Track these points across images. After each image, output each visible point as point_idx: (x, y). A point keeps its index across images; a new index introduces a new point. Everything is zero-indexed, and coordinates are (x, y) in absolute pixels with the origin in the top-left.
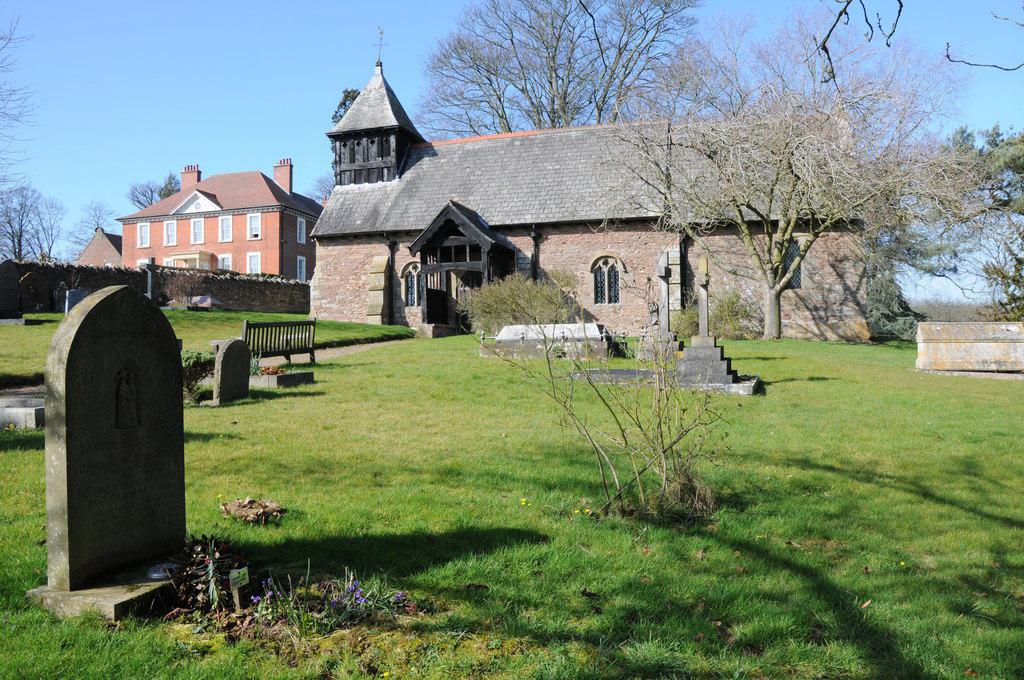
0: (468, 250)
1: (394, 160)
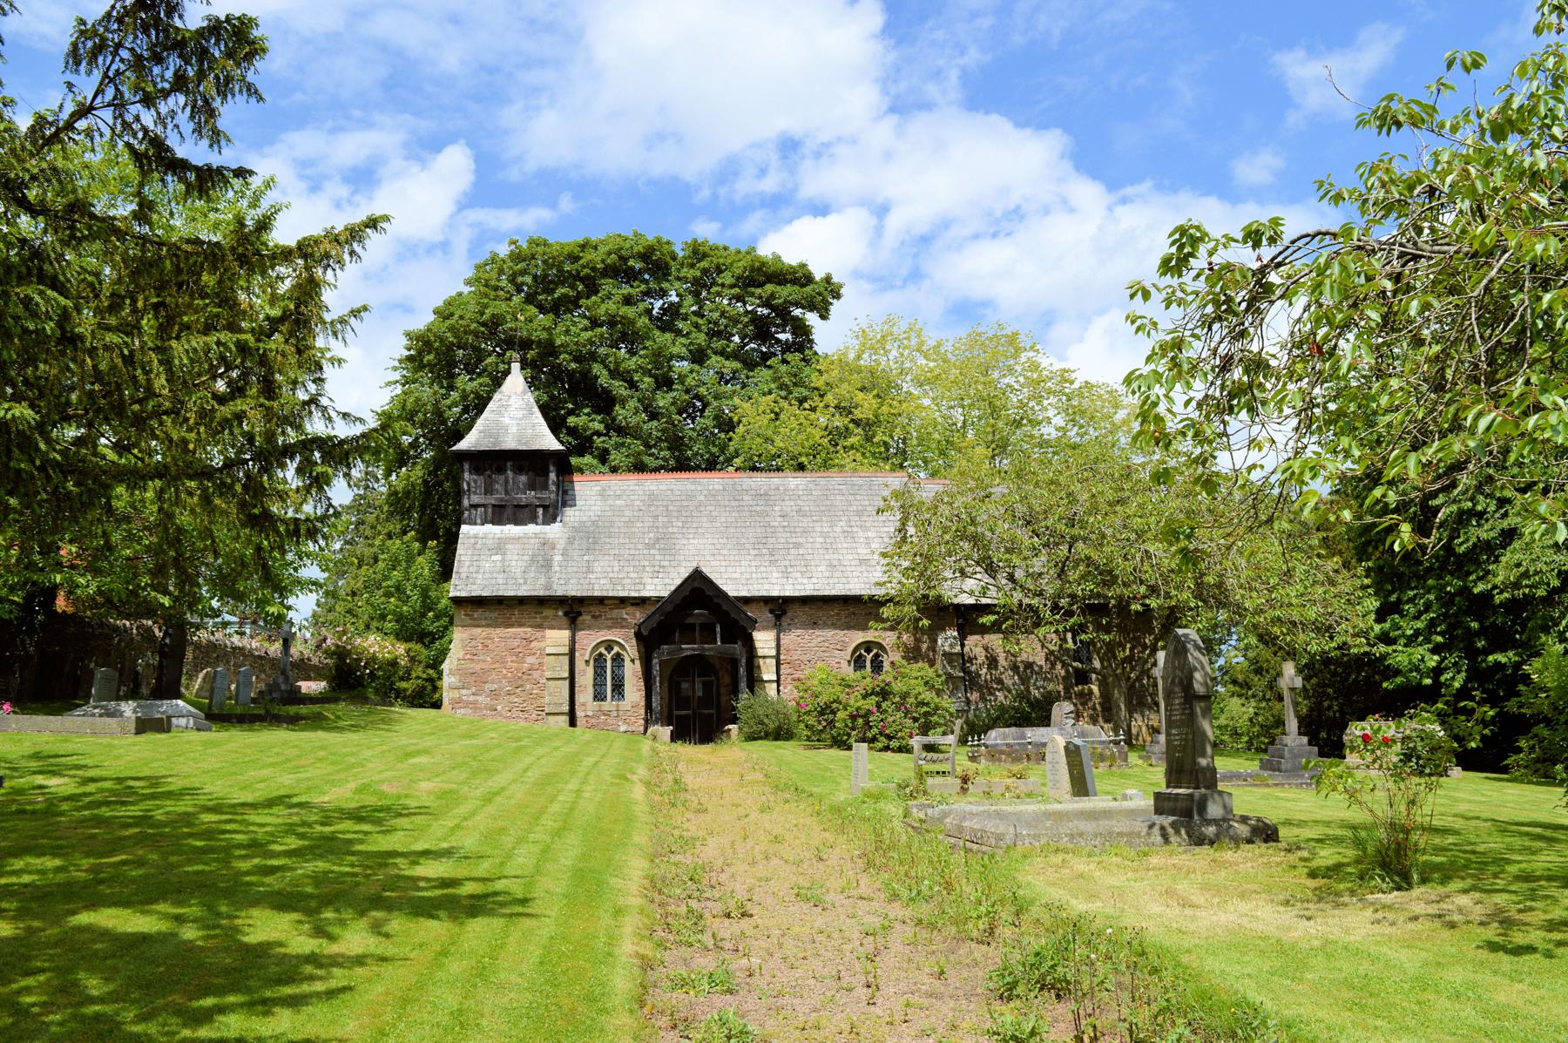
0: (718, 629)
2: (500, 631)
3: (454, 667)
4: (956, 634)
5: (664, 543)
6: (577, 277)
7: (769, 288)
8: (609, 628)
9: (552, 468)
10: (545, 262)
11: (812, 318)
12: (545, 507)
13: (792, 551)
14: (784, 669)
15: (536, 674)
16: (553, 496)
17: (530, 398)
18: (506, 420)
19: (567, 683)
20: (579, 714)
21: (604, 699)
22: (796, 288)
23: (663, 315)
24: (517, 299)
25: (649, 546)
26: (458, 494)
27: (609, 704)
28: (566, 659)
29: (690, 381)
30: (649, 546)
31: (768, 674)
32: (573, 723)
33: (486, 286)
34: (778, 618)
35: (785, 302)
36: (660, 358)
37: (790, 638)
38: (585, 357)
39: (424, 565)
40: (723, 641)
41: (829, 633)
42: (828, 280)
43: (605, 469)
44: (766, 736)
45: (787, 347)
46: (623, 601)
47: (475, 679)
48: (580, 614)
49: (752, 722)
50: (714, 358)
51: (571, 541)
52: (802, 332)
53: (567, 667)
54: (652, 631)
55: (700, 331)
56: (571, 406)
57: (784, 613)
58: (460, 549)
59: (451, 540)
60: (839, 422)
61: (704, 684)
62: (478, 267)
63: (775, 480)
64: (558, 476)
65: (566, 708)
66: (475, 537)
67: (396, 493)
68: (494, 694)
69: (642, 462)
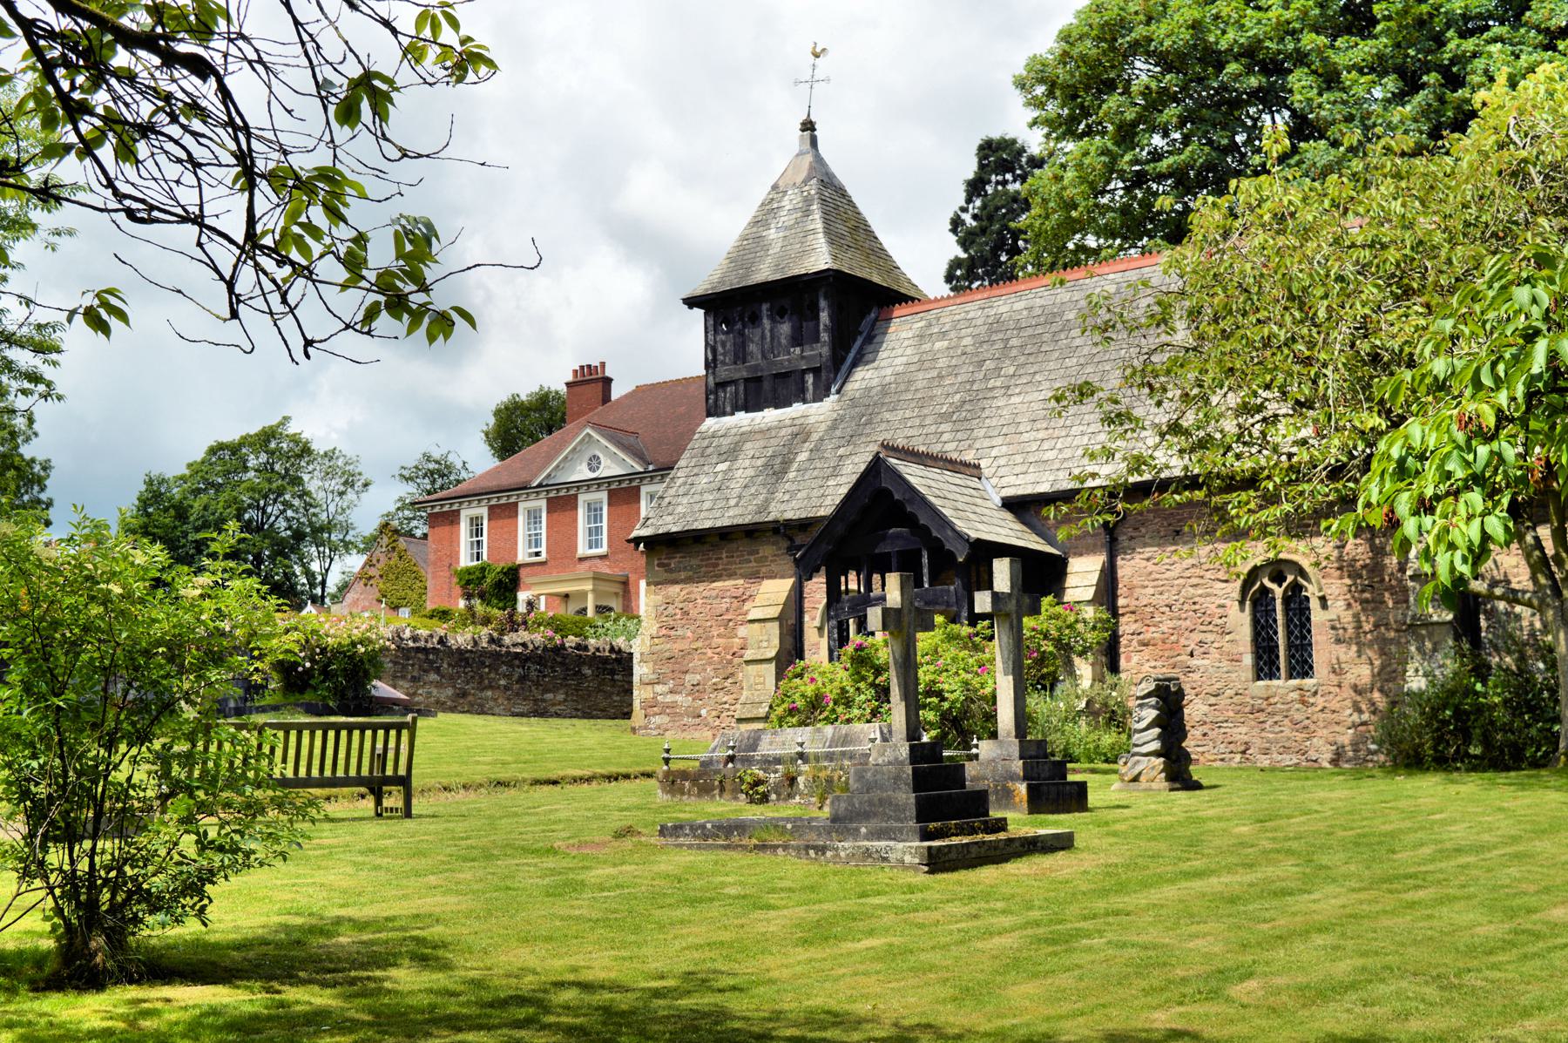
0: (925, 560)
1: (825, 351)
2: (701, 590)
3: (646, 650)
9: (823, 303)
12: (816, 371)
68: (697, 690)
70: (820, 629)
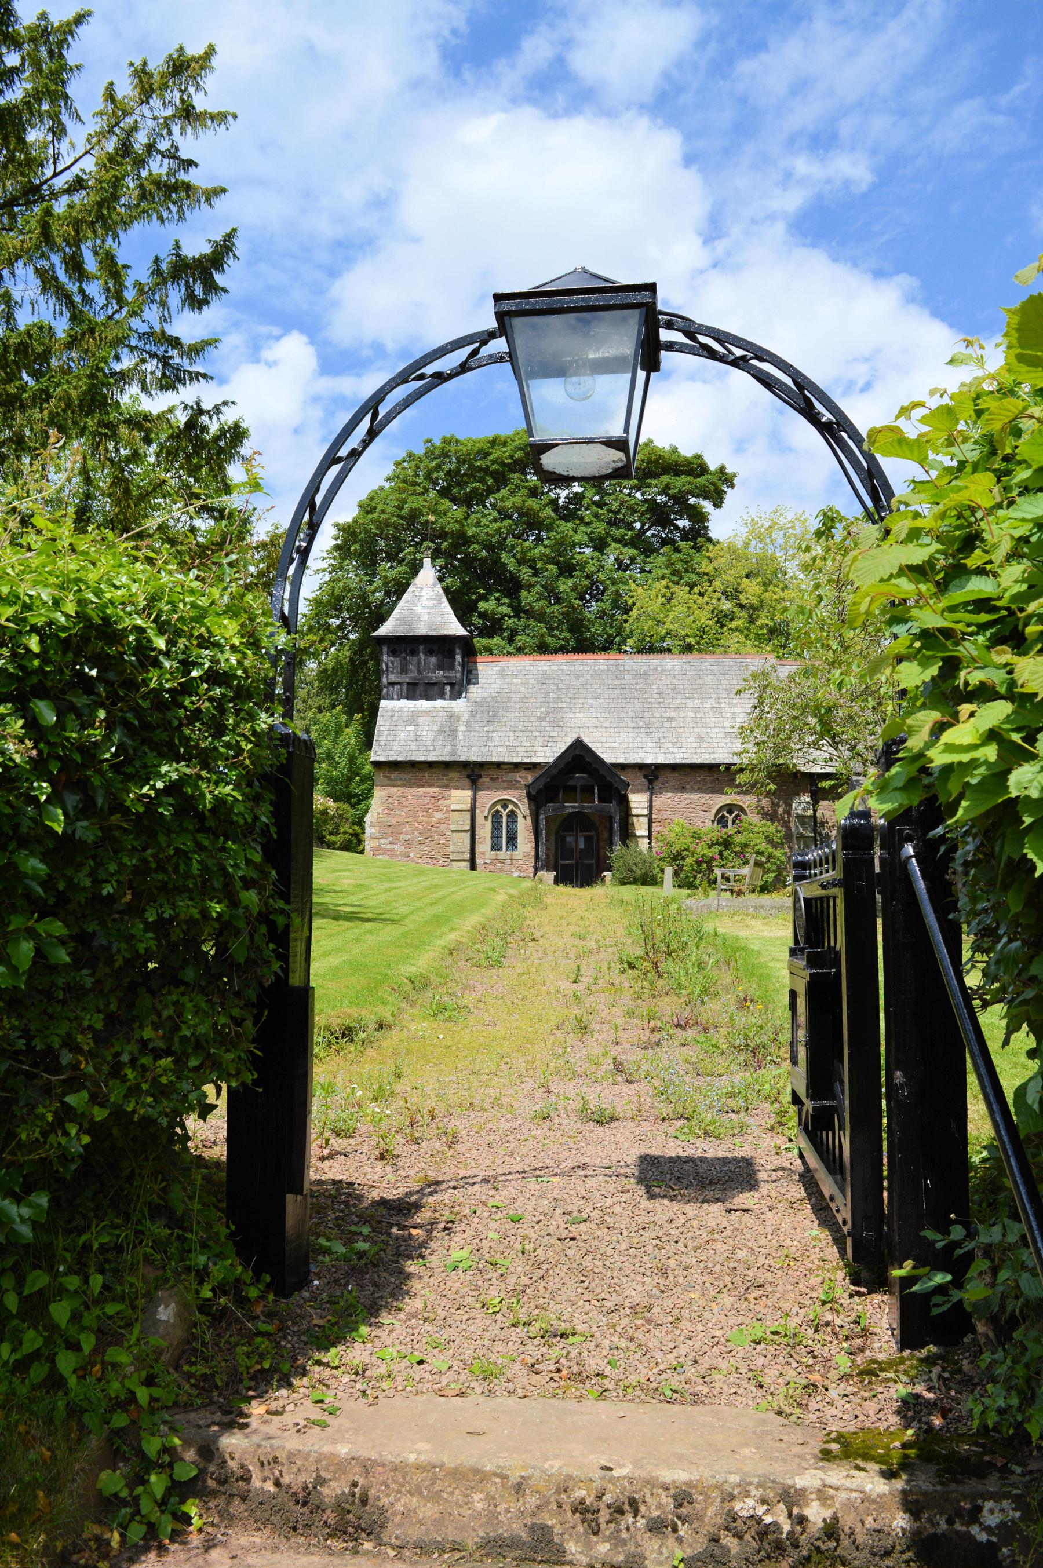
2: (413, 791)
3: (374, 820)
4: (808, 799)
5: (553, 716)
6: (486, 470)
7: (665, 479)
8: (505, 789)
10: (458, 458)
11: (707, 506)
12: (452, 685)
13: (666, 724)
14: (655, 827)
15: (443, 827)
16: (459, 675)
17: (439, 589)
18: (419, 609)
19: (468, 835)
20: (479, 861)
21: (500, 849)
22: (691, 479)
23: (570, 503)
24: (432, 494)
25: (542, 719)
26: (379, 674)
27: (504, 854)
28: (468, 815)
29: (591, 568)
30: (542, 719)
31: (641, 830)
32: (473, 867)
33: (405, 481)
34: (651, 782)
35: (680, 491)
36: (562, 546)
37: (661, 800)
38: (495, 548)
39: (350, 735)
40: (601, 800)
41: (695, 797)
42: (722, 470)
43: (511, 649)
44: (635, 882)
45: (685, 535)
46: (517, 766)
47: (392, 831)
48: (480, 776)
49: (622, 870)
50: (614, 545)
51: (473, 714)
52: (699, 518)
53: (468, 822)
54: (540, 791)
55: (600, 520)
56: (482, 591)
57: (657, 778)
58: (380, 721)
59: (373, 712)
60: (727, 606)
61: (587, 838)
62: (397, 464)
63: (653, 661)
64: (463, 658)
65: (467, 856)
66: (393, 710)
67: (326, 670)
68: (408, 843)
69: (545, 643)
70: (486, 817)
